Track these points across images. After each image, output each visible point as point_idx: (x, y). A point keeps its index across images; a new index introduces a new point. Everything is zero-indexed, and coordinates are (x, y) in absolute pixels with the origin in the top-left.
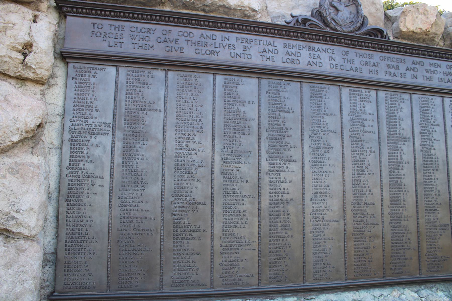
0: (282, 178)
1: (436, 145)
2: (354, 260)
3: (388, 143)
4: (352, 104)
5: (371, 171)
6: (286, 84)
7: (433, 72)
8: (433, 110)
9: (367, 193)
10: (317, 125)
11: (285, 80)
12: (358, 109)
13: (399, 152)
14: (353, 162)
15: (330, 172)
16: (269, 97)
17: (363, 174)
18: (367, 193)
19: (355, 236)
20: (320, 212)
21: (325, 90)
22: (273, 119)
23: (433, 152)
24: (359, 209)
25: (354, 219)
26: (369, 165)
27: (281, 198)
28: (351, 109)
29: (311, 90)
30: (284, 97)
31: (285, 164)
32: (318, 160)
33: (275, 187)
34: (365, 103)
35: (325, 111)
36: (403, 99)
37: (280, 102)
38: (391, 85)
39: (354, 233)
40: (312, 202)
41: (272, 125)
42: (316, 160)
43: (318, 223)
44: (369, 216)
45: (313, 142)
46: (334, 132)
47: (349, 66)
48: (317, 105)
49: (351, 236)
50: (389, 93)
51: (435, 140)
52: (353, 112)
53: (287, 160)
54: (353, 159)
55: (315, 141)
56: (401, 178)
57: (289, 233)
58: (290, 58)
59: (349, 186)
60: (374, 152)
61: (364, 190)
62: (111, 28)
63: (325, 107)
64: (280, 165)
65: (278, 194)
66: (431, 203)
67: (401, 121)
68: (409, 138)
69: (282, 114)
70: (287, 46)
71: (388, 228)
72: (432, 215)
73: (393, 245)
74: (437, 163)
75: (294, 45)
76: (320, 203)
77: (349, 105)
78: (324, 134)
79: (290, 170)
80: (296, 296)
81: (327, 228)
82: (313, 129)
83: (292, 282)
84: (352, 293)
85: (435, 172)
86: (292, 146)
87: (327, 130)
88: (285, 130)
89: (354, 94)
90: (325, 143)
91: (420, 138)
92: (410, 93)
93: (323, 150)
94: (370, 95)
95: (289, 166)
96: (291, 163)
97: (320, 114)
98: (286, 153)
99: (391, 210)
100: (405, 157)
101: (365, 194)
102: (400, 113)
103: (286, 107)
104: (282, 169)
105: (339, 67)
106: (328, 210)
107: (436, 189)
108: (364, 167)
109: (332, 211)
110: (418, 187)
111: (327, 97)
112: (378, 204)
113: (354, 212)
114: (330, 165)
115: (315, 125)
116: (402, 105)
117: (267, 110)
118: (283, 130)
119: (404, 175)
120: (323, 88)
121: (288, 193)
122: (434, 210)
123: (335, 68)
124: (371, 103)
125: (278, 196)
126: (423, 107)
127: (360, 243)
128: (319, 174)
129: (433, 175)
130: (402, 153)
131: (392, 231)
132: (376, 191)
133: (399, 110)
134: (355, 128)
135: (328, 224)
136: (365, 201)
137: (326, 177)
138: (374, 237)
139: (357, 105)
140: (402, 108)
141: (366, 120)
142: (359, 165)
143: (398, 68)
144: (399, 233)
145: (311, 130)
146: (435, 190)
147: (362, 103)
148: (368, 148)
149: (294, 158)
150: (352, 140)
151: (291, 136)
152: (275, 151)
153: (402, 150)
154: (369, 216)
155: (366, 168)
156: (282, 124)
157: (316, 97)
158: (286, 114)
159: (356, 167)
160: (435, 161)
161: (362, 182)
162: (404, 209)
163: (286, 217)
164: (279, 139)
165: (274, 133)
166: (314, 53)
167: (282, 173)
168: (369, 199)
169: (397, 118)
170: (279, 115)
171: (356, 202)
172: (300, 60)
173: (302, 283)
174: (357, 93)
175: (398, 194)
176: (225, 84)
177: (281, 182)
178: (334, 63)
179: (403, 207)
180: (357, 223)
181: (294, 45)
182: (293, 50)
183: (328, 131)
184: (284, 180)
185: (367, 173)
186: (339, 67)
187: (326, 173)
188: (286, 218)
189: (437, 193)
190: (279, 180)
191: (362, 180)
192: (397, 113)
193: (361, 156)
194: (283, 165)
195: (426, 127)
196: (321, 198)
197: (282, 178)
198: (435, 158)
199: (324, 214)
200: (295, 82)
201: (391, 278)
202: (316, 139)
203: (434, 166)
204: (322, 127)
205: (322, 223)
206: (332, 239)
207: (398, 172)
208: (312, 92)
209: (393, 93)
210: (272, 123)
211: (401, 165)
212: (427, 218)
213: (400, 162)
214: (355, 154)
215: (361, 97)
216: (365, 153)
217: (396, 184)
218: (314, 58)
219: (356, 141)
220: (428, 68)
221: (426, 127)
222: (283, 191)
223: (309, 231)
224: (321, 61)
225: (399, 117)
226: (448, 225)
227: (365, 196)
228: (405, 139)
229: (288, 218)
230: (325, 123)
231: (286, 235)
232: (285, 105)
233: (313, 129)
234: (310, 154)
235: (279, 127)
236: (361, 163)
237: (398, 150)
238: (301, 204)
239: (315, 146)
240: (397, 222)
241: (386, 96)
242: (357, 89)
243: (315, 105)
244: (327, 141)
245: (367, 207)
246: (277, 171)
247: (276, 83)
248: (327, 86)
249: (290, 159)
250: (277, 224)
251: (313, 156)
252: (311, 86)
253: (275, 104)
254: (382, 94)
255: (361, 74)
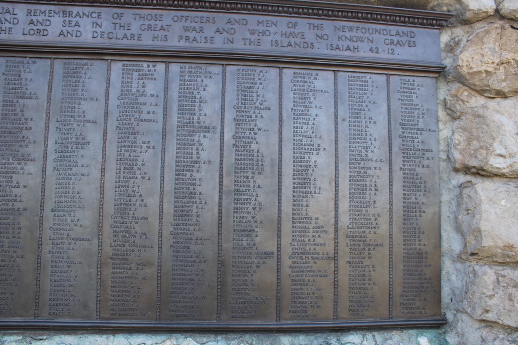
0: (15, 182)
1: (261, 137)
2: (111, 293)
3: (178, 135)
4: (126, 83)
5: (145, 173)
6: (30, 62)
7: (263, 33)
8: (261, 87)
9: (138, 204)
10: (69, 114)
11: (29, 57)
12: (134, 90)
13: (194, 148)
14: (119, 162)
15: (83, 175)
16: (6, 79)
17: (133, 177)
18: (138, 204)
19: (114, 262)
20: (64, 227)
21: (85, 67)
22: (8, 108)
23: (254, 146)
24: (123, 225)
25: (115, 238)
26: (143, 165)
27: (11, 207)
28: (122, 90)
29: (65, 68)
30: (26, 79)
31: (19, 164)
32: (66, 159)
33: (4, 194)
34: (146, 82)
35: (82, 94)
36: (210, 73)
37: (19, 86)
38: (185, 54)
39: (114, 256)
40: (54, 213)
41: (6, 115)
42: (63, 159)
43: (60, 241)
44: (138, 235)
45: (60, 136)
46: (93, 122)
47: (120, 33)
48: (71, 87)
49: (108, 260)
50: (187, 65)
51: (259, 130)
52: (125, 95)
53: (23, 159)
54: (119, 157)
55: (64, 134)
56: (195, 184)
57: (19, 252)
58: (35, 28)
59: (110, 194)
60: (154, 148)
61: (134, 199)
62: (245, 42)
63: (83, 90)
64: (13, 166)
65: (8, 202)
66: (244, 220)
67: (202, 105)
68: (214, 128)
69: (21, 101)
70: (32, 13)
71: (167, 253)
72: (245, 239)
73: (174, 277)
74: (260, 163)
75: (43, 11)
76: (65, 215)
77: (120, 85)
78: (78, 125)
79: (26, 172)
80: (22, 334)
81: (73, 249)
82: (62, 119)
83: (19, 316)
84: (105, 336)
85: (256, 176)
86: (32, 141)
87: (83, 119)
88: (24, 121)
89: (130, 70)
90: (78, 137)
91: (234, 127)
92: (223, 65)
93: (75, 146)
94: (155, 70)
95: (25, 167)
96: (28, 162)
97: (75, 99)
98: (23, 150)
99: (175, 229)
100: (204, 155)
101: (135, 205)
102: (202, 92)
103: (28, 92)
104: (15, 170)
105: (105, 36)
106: (76, 225)
107: (256, 200)
108: (135, 168)
109: (81, 226)
110: (224, 196)
111: (88, 76)
112: (154, 220)
113: (115, 229)
114: (83, 166)
115: (66, 114)
116: (207, 81)
117: (1, 97)
118: (21, 122)
119: (200, 180)
120: (83, 65)
121: (21, 201)
122: (250, 231)
123: (99, 37)
124: (154, 81)
125: (7, 205)
126: (244, 83)
127: (122, 270)
128: (67, 177)
129: (252, 181)
130: (200, 148)
131: (175, 258)
132: (153, 200)
133: (202, 89)
134: (127, 116)
135: (75, 244)
136: (134, 214)
137: (76, 182)
138: (144, 264)
139: (134, 85)
140: (206, 86)
141: (145, 104)
142: (128, 166)
143: (201, 30)
144: (185, 261)
145: (59, 120)
146: (253, 203)
147: (141, 82)
148: (144, 143)
149: (33, 157)
150: (120, 131)
151: (31, 128)
152: (8, 148)
153: (201, 145)
154: (138, 235)
155: (139, 169)
156: (20, 114)
157: (71, 77)
158: (26, 100)
159: (122, 168)
160: (258, 160)
161: (130, 190)
162: (197, 228)
163: (17, 231)
164: (14, 133)
165: (9, 125)
166: (71, 19)
167: (14, 176)
168: (140, 212)
169: (197, 101)
170: (17, 102)
171: (119, 215)
172: (49, 30)
173: (33, 318)
174: (135, 68)
175: (188, 207)
176: (294, 108)
177: (12, 187)
178: (99, 30)
179: (196, 225)
180: (118, 243)
181: (43, 11)
182: (40, 18)
183: (84, 121)
184: (17, 184)
185: (139, 177)
186: (105, 36)
187: (76, 176)
188: (16, 233)
189: (257, 207)
190: (10, 184)
191: (131, 185)
192: (198, 93)
193: (133, 154)
194: (17, 166)
195: (246, 112)
196: (66, 209)
197: (15, 182)
198: (258, 156)
199: (69, 230)
200: (43, 60)
201: (169, 322)
202: (66, 132)
203: (255, 168)
204: (76, 116)
205: (66, 241)
206: (80, 263)
207: (191, 175)
208: (67, 70)
209: (193, 65)
210: (7, 112)
211: (197, 165)
212: (235, 242)
213: (196, 162)
214: (123, 151)
215: (141, 73)
216: (139, 150)
217: (186, 191)
218: (71, 25)
219: (125, 133)
220: (255, 27)
221: (246, 112)
222: (14, 198)
223: (47, 251)
224: (79, 29)
225: (201, 98)
226: (273, 253)
227: (133, 208)
228: (207, 129)
229: (19, 233)
230: (81, 111)
231: (15, 255)
232: (27, 89)
233: (62, 119)
234: (56, 151)
235: (16, 117)
236: (131, 162)
237: (194, 144)
238: (38, 215)
239: (64, 141)
240: (183, 245)
241: (182, 70)
242: (135, 63)
243: (68, 88)
244: (81, 134)
245: (136, 223)
246: (7, 173)
247: (17, 61)
248: (90, 62)
249: (27, 157)
250: (4, 240)
251: (60, 154)
252: (65, 64)
253: (13, 88)
254: (175, 68)
255: (139, 43)
